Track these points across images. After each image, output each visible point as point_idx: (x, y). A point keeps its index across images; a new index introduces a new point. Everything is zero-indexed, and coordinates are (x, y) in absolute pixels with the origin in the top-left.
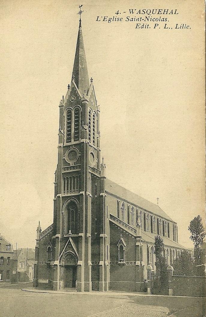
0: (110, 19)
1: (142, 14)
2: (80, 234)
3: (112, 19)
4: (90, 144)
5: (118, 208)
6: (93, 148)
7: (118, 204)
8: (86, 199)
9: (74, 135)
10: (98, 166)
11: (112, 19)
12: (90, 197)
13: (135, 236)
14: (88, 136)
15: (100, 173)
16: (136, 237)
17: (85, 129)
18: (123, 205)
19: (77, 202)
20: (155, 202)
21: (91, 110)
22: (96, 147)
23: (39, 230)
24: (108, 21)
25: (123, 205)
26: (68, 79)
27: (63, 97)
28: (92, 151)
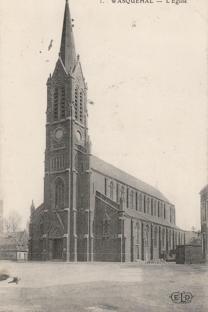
0: (177, 1)
1: (123, 2)
2: (66, 209)
3: (179, 1)
4: (76, 122)
5: (106, 185)
6: (80, 127)
7: (106, 181)
8: (72, 174)
9: (58, 111)
10: (85, 145)
11: (179, 1)
12: (76, 173)
13: (118, 210)
14: (74, 114)
15: (86, 151)
16: (119, 212)
17: (71, 107)
18: (123, 188)
19: (62, 178)
20: (155, 187)
21: (78, 87)
22: (83, 126)
23: (32, 208)
24: (175, 3)
25: (123, 188)
26: (54, 56)
27: (50, 75)
28: (79, 129)
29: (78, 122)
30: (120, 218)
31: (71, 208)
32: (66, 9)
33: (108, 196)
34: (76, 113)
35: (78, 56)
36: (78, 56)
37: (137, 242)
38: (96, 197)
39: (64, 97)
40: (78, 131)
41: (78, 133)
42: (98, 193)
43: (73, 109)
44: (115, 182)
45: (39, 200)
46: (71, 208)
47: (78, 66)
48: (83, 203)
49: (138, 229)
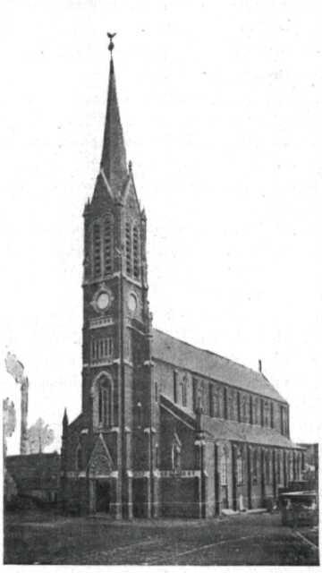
4: (128, 279)
14: (125, 267)
29: (132, 279)
30: (197, 443)
31: (123, 428)
32: (105, 163)
33: (179, 405)
34: (128, 263)
35: (130, 163)
36: (130, 166)
37: (225, 479)
38: (161, 408)
39: (111, 228)
40: (132, 295)
41: (132, 299)
42: (163, 400)
43: (124, 258)
44: (189, 376)
45: (75, 412)
46: (123, 428)
47: (130, 182)
48: (142, 414)
49: (227, 457)
